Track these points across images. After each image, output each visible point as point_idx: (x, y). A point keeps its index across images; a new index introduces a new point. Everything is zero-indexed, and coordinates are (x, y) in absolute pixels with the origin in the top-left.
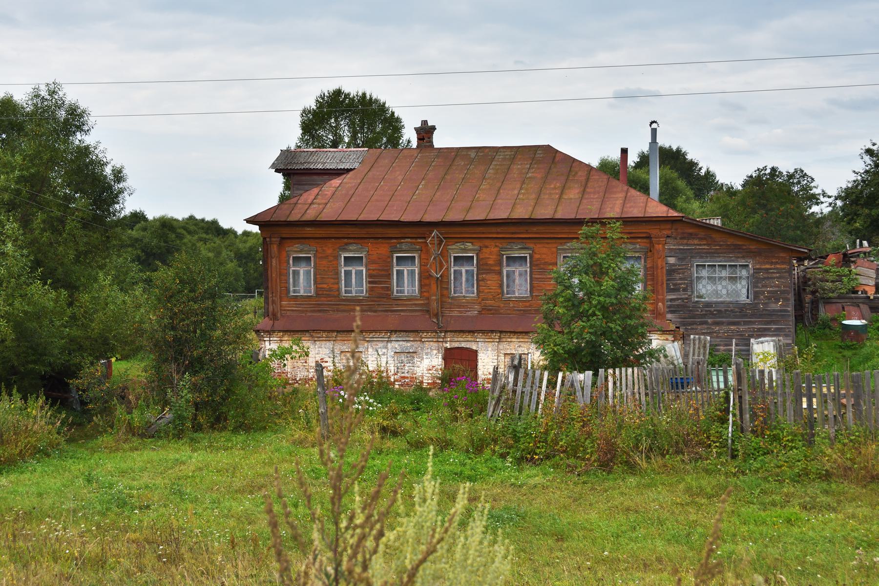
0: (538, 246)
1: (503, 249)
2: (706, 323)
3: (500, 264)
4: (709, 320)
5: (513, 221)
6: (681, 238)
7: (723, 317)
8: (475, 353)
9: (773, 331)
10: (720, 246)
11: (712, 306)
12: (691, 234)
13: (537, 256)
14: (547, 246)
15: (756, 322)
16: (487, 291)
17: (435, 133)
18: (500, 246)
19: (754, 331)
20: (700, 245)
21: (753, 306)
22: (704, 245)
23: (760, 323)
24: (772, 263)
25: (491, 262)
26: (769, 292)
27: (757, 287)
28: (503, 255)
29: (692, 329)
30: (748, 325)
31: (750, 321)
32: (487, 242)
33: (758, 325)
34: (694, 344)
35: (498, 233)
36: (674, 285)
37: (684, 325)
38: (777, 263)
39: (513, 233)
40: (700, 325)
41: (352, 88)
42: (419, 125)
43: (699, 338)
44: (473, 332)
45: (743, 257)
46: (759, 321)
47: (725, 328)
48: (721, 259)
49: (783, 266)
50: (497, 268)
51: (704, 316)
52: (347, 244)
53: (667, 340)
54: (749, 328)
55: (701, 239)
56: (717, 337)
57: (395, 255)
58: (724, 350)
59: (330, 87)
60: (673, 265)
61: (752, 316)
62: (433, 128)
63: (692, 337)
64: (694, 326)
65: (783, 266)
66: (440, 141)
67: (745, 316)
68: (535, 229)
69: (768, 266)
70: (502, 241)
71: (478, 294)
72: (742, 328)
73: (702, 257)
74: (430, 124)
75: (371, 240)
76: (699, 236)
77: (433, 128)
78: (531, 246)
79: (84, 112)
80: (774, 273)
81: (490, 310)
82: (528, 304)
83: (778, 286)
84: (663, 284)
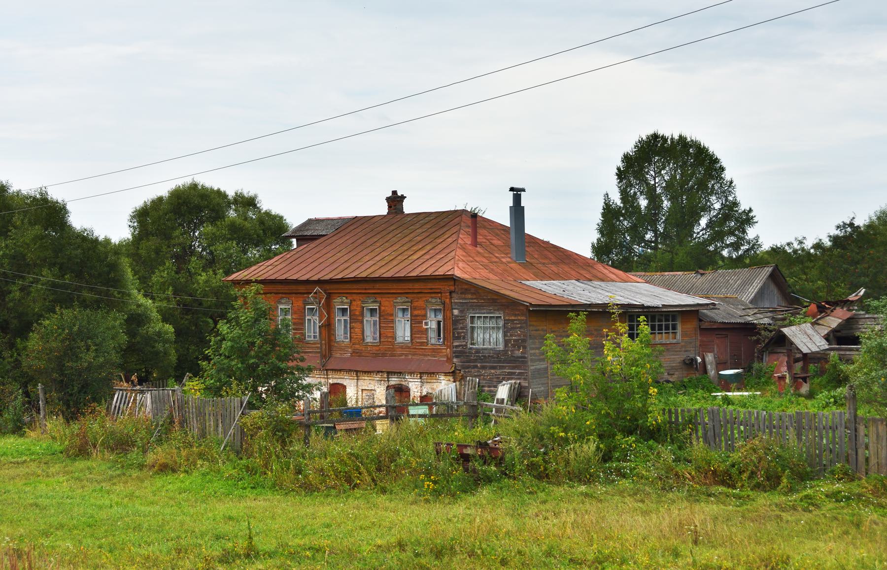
0: (384, 299)
1: (364, 302)
2: (476, 367)
3: (362, 315)
4: (479, 365)
5: (359, 279)
6: (461, 293)
7: (487, 362)
8: (345, 387)
9: (517, 375)
10: (484, 299)
11: (479, 353)
12: (466, 289)
13: (383, 308)
14: (388, 299)
15: (506, 367)
16: (355, 337)
17: (405, 201)
18: (362, 299)
19: (506, 375)
20: (472, 299)
21: (505, 352)
22: (475, 299)
23: (510, 368)
24: (515, 315)
25: (357, 313)
26: (514, 340)
27: (507, 336)
28: (364, 307)
29: (469, 372)
30: (502, 369)
31: (503, 366)
32: (355, 296)
33: (508, 369)
34: (469, 383)
35: (358, 289)
36: (458, 333)
37: (464, 368)
38: (518, 315)
39: (366, 289)
40: (473, 368)
41: (671, 130)
42: (390, 194)
43: (472, 380)
44: (340, 370)
45: (498, 310)
46: (509, 366)
47: (488, 371)
48: (485, 311)
49: (522, 318)
50: (361, 318)
51: (475, 361)
52: (282, 298)
53: (449, 380)
54: (503, 372)
55: (473, 294)
56: (484, 379)
57: (307, 307)
58: (488, 391)
59: (645, 133)
60: (457, 316)
61: (505, 361)
62: (403, 197)
63: (468, 378)
64: (470, 370)
65: (522, 318)
66: (409, 207)
67: (500, 362)
68: (377, 286)
69: (513, 318)
70: (363, 295)
71: (350, 339)
72: (498, 372)
73: (473, 310)
74: (399, 194)
75: (294, 295)
76: (472, 291)
77: (403, 197)
78: (378, 299)
79: (236, 193)
80: (517, 324)
81: (357, 353)
82: (377, 348)
83: (519, 335)
84: (450, 332)
